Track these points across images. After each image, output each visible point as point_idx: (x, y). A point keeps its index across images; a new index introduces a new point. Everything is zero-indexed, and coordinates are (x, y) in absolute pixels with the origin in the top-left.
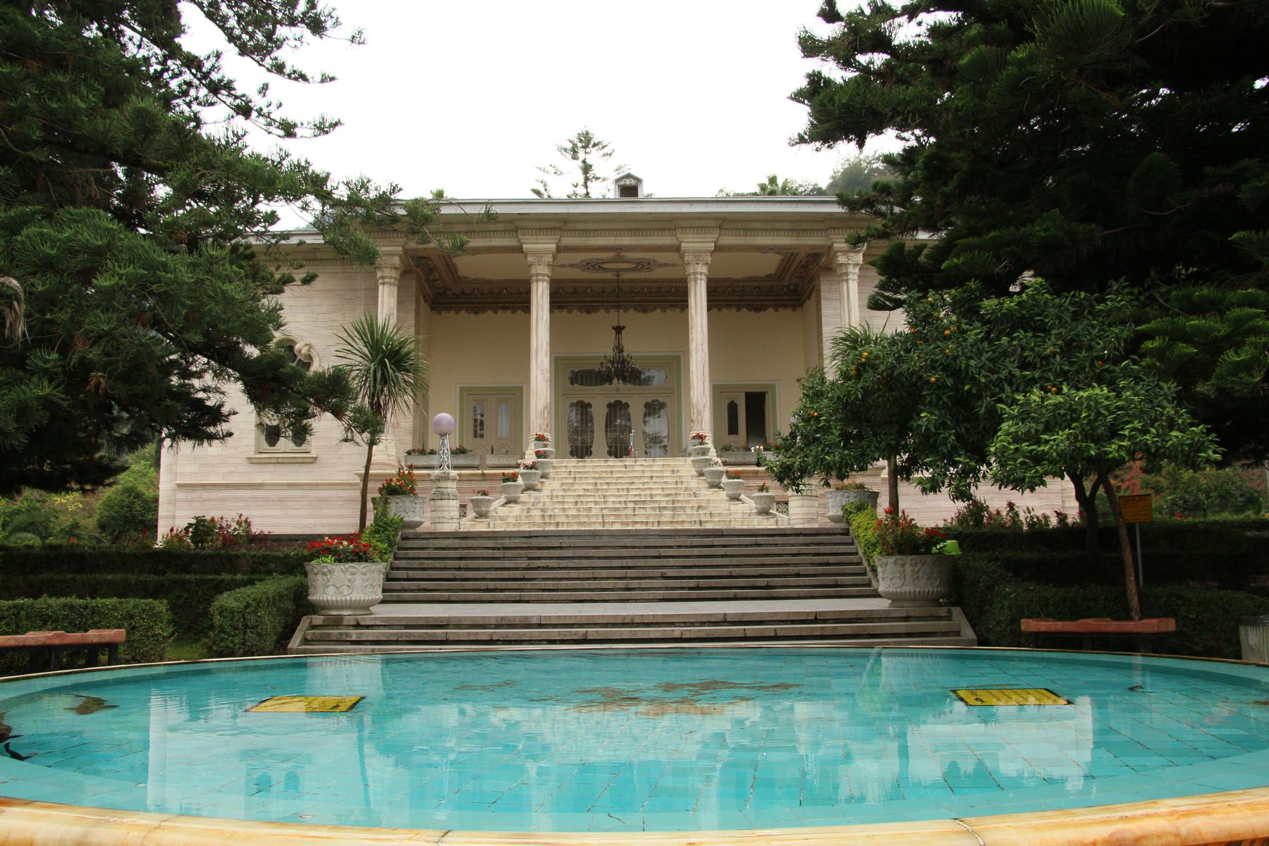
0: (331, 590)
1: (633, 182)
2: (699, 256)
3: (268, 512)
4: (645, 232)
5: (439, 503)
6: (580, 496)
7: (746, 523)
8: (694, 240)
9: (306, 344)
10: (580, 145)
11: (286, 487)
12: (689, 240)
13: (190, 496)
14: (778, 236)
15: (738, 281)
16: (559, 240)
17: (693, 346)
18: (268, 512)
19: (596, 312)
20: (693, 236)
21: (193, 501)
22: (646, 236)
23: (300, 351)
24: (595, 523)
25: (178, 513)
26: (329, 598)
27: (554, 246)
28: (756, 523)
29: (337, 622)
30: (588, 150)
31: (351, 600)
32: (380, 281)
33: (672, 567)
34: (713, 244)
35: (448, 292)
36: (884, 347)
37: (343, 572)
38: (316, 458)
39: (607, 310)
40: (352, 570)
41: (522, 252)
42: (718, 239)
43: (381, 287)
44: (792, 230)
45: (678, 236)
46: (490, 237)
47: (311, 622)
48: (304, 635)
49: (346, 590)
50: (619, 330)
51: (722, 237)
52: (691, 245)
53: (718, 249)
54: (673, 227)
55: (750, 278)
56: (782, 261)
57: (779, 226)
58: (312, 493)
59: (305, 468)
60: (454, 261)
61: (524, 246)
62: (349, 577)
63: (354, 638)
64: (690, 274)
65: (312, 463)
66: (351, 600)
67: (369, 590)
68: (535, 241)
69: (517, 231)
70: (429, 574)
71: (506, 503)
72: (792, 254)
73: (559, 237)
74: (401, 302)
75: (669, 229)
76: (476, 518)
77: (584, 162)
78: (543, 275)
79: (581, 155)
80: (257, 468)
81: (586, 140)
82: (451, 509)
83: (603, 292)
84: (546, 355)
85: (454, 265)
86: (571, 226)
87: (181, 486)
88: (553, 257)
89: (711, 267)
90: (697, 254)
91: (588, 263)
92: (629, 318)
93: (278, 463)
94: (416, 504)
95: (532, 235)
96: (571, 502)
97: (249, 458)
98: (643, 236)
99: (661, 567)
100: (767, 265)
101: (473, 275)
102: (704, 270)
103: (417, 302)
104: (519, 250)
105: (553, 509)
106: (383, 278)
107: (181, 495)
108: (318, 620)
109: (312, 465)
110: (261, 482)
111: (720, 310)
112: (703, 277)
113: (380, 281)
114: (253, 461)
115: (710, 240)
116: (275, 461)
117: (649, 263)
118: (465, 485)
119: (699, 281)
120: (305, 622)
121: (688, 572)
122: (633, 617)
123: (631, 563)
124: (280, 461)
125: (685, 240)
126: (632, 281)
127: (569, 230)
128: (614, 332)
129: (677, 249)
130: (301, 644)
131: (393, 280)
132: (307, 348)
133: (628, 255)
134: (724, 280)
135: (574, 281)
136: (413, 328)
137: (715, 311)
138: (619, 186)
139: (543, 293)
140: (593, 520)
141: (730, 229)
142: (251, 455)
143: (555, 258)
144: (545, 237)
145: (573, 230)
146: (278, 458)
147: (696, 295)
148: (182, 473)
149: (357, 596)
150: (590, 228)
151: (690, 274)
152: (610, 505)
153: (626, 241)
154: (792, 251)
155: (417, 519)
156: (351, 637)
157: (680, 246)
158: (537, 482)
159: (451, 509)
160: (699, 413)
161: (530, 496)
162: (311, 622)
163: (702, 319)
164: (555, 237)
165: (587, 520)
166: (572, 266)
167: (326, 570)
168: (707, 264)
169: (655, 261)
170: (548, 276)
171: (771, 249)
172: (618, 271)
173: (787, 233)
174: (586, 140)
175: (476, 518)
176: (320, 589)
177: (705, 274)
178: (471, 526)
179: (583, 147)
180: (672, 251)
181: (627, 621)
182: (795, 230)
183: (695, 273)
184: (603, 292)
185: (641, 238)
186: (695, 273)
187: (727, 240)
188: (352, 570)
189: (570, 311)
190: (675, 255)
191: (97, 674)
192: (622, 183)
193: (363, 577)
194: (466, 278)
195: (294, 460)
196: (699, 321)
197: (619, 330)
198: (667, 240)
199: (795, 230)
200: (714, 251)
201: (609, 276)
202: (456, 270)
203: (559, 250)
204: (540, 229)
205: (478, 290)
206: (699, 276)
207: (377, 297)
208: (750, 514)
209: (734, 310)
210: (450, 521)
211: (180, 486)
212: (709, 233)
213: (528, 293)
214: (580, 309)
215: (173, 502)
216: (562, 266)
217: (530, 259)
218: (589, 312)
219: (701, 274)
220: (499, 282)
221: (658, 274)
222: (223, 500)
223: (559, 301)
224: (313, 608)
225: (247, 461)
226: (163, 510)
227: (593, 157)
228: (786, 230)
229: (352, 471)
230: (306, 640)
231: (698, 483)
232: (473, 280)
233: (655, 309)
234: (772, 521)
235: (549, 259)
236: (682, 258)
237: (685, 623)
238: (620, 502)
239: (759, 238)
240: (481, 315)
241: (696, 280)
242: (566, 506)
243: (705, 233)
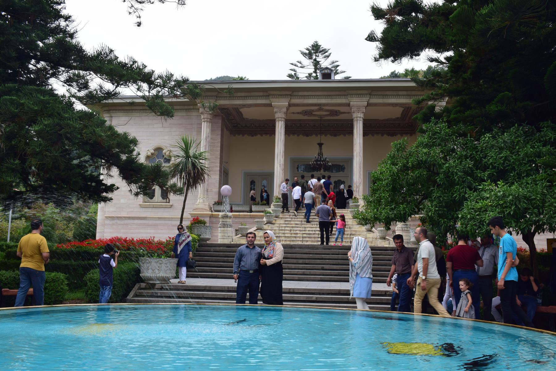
0: (150, 271)
1: (329, 71)
2: (359, 109)
3: (149, 231)
4: (299, 97)
5: (226, 229)
6: (293, 227)
7: (373, 243)
8: (356, 101)
9: (168, 150)
10: (313, 51)
11: (157, 219)
12: (355, 101)
13: (111, 222)
14: (399, 98)
15: (382, 120)
16: (290, 101)
17: (355, 154)
18: (149, 231)
19: (311, 136)
20: (357, 98)
21: (113, 224)
22: (333, 98)
23: (165, 154)
24: (298, 241)
25: (106, 230)
26: (149, 275)
27: (287, 103)
28: (379, 243)
29: (153, 286)
30: (317, 54)
31: (159, 277)
32: (203, 120)
33: (328, 264)
34: (366, 103)
35: (239, 126)
36: (492, 156)
37: (156, 262)
38: (172, 205)
39: (317, 135)
40: (161, 262)
41: (272, 106)
42: (369, 100)
43: (203, 123)
44: (407, 95)
45: (349, 98)
46: (256, 99)
47: (140, 286)
48: (135, 292)
49: (157, 271)
50: (320, 145)
51: (371, 99)
52: (355, 103)
53: (369, 105)
54: (346, 94)
55: (388, 119)
56: (403, 111)
57: (400, 93)
58: (169, 222)
59: (167, 210)
60: (240, 111)
61: (273, 103)
62: (159, 265)
63: (159, 295)
64: (354, 118)
65: (170, 207)
66: (159, 277)
67: (168, 272)
68: (278, 101)
69: (269, 96)
70: (339, 262)
71: (256, 230)
72: (409, 107)
73: (289, 99)
74: (213, 130)
75: (344, 95)
76: (241, 236)
77: (315, 60)
78: (281, 118)
79: (314, 57)
80: (144, 210)
81: (316, 49)
82: (228, 232)
83: (315, 126)
84: (282, 157)
85: (241, 112)
86: (296, 93)
87: (107, 218)
88: (287, 109)
89: (365, 114)
90: (359, 107)
91: (306, 112)
92: (326, 139)
93: (154, 207)
94: (207, 229)
95: (276, 98)
96: (288, 230)
97: (140, 205)
98: (331, 98)
99: (322, 264)
100: (397, 113)
101: (250, 117)
102: (362, 115)
103: (222, 131)
104: (270, 105)
105: (279, 233)
106: (204, 119)
107: (108, 222)
108: (143, 285)
109: (170, 209)
110: (145, 216)
111: (373, 135)
112: (361, 119)
113: (203, 120)
114: (142, 206)
115: (365, 100)
116: (152, 206)
117: (336, 112)
118: (237, 220)
119: (359, 121)
120: (137, 286)
121: (335, 267)
122: (294, 289)
123: (307, 261)
124: (155, 206)
125: (352, 100)
126: (329, 120)
127: (295, 95)
128: (318, 146)
129: (349, 105)
130: (133, 297)
131: (209, 120)
132: (168, 152)
133: (325, 108)
134: (375, 120)
135: (300, 120)
136: (220, 143)
137: (286, 135)
138: (322, 73)
139: (281, 126)
140: (298, 239)
141: (375, 95)
142: (141, 203)
143: (287, 109)
144: (284, 99)
145: (297, 96)
146: (153, 205)
147: (357, 128)
148: (108, 211)
149: (162, 274)
150: (305, 95)
151: (354, 118)
152: (307, 232)
153: (323, 101)
154: (408, 106)
155: (207, 237)
156: (157, 294)
157: (350, 104)
158: (272, 220)
159: (228, 232)
160: (357, 187)
161: (268, 227)
162: (140, 286)
163: (360, 140)
164: (288, 99)
165: (294, 239)
166: (298, 113)
167: (148, 261)
168: (363, 112)
169: (339, 111)
170: (284, 118)
171: (396, 105)
172: (320, 116)
173: (261, 97)
174: (316, 49)
175: (241, 236)
176: (145, 271)
177: (362, 118)
178: (238, 240)
179: (314, 53)
180: (346, 106)
181: (291, 291)
182: (409, 95)
183: (357, 117)
184: (315, 126)
185: (330, 100)
186: (357, 117)
187: (374, 100)
188: (161, 262)
189: (298, 135)
190: (347, 108)
191: (150, 305)
192: (323, 72)
193: (165, 265)
194: (246, 118)
195: (161, 206)
196: (358, 141)
197: (320, 145)
198: (343, 101)
199: (409, 95)
200: (367, 106)
201: (317, 118)
202: (242, 115)
203: (290, 105)
204: (280, 95)
205: (267, 125)
206: (359, 119)
207: (201, 128)
208: (376, 239)
209: (241, 135)
210: (228, 238)
211: (107, 217)
212: (364, 97)
213: (275, 123)
214: (331, 135)
215: (104, 225)
216: (293, 113)
217: (275, 110)
218: (307, 136)
219: (360, 117)
220: (263, 121)
221: (341, 117)
222: (127, 224)
223: (290, 130)
224: (141, 280)
225: (139, 206)
226: (98, 230)
227: (320, 58)
228: (404, 95)
229: (187, 212)
230: (136, 295)
231: (353, 222)
232: (251, 120)
233: (340, 135)
234: (387, 242)
235: (285, 110)
236: (351, 109)
237: (320, 293)
238: (312, 231)
239: (390, 99)
240: (255, 137)
241: (357, 120)
242: (286, 232)
243: (362, 97)
